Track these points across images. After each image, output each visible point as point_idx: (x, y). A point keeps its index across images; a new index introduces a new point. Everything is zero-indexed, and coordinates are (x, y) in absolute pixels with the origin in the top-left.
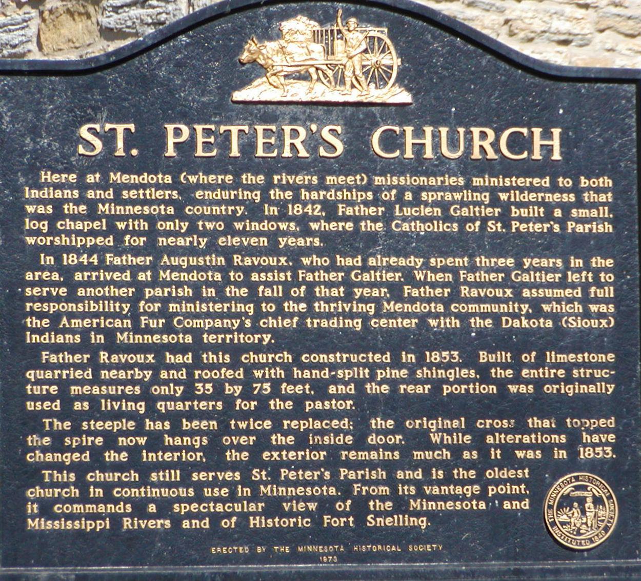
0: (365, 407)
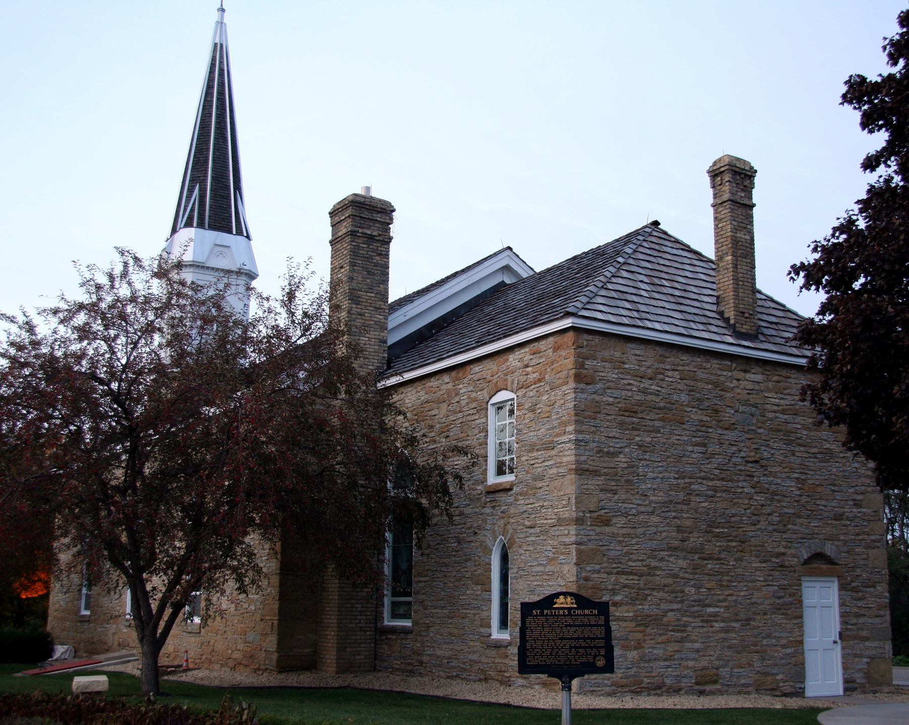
0: (571, 648)
